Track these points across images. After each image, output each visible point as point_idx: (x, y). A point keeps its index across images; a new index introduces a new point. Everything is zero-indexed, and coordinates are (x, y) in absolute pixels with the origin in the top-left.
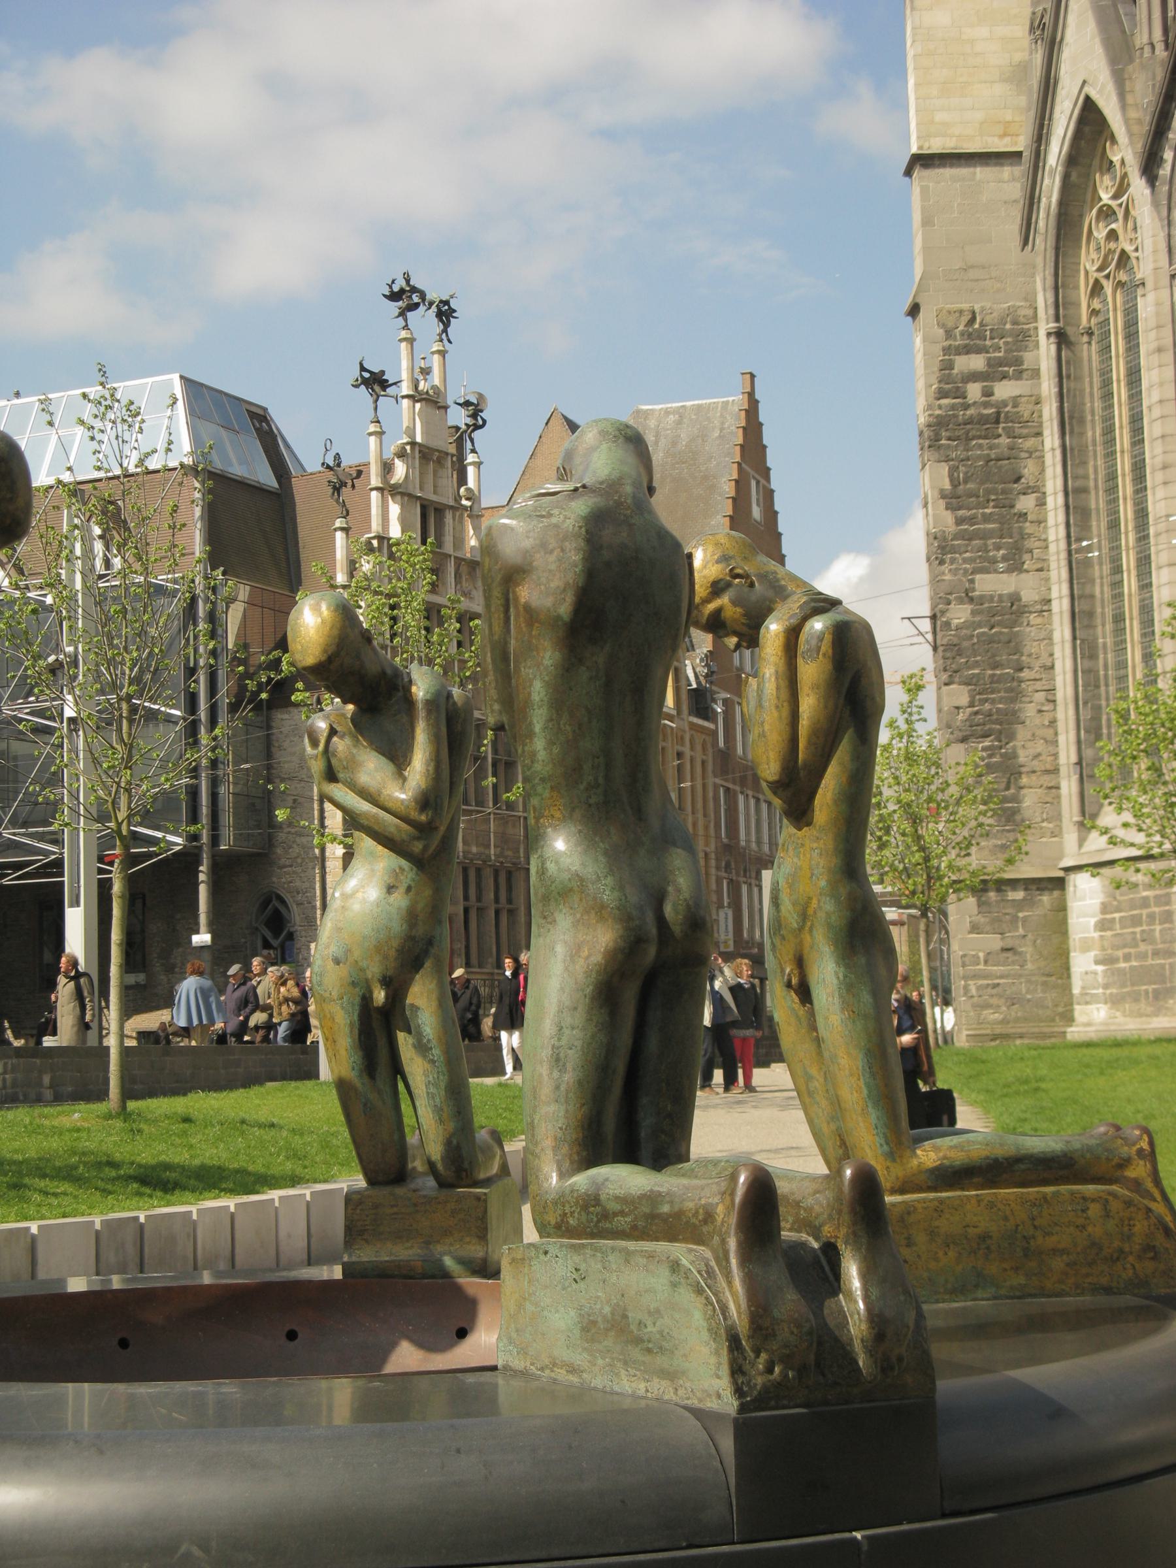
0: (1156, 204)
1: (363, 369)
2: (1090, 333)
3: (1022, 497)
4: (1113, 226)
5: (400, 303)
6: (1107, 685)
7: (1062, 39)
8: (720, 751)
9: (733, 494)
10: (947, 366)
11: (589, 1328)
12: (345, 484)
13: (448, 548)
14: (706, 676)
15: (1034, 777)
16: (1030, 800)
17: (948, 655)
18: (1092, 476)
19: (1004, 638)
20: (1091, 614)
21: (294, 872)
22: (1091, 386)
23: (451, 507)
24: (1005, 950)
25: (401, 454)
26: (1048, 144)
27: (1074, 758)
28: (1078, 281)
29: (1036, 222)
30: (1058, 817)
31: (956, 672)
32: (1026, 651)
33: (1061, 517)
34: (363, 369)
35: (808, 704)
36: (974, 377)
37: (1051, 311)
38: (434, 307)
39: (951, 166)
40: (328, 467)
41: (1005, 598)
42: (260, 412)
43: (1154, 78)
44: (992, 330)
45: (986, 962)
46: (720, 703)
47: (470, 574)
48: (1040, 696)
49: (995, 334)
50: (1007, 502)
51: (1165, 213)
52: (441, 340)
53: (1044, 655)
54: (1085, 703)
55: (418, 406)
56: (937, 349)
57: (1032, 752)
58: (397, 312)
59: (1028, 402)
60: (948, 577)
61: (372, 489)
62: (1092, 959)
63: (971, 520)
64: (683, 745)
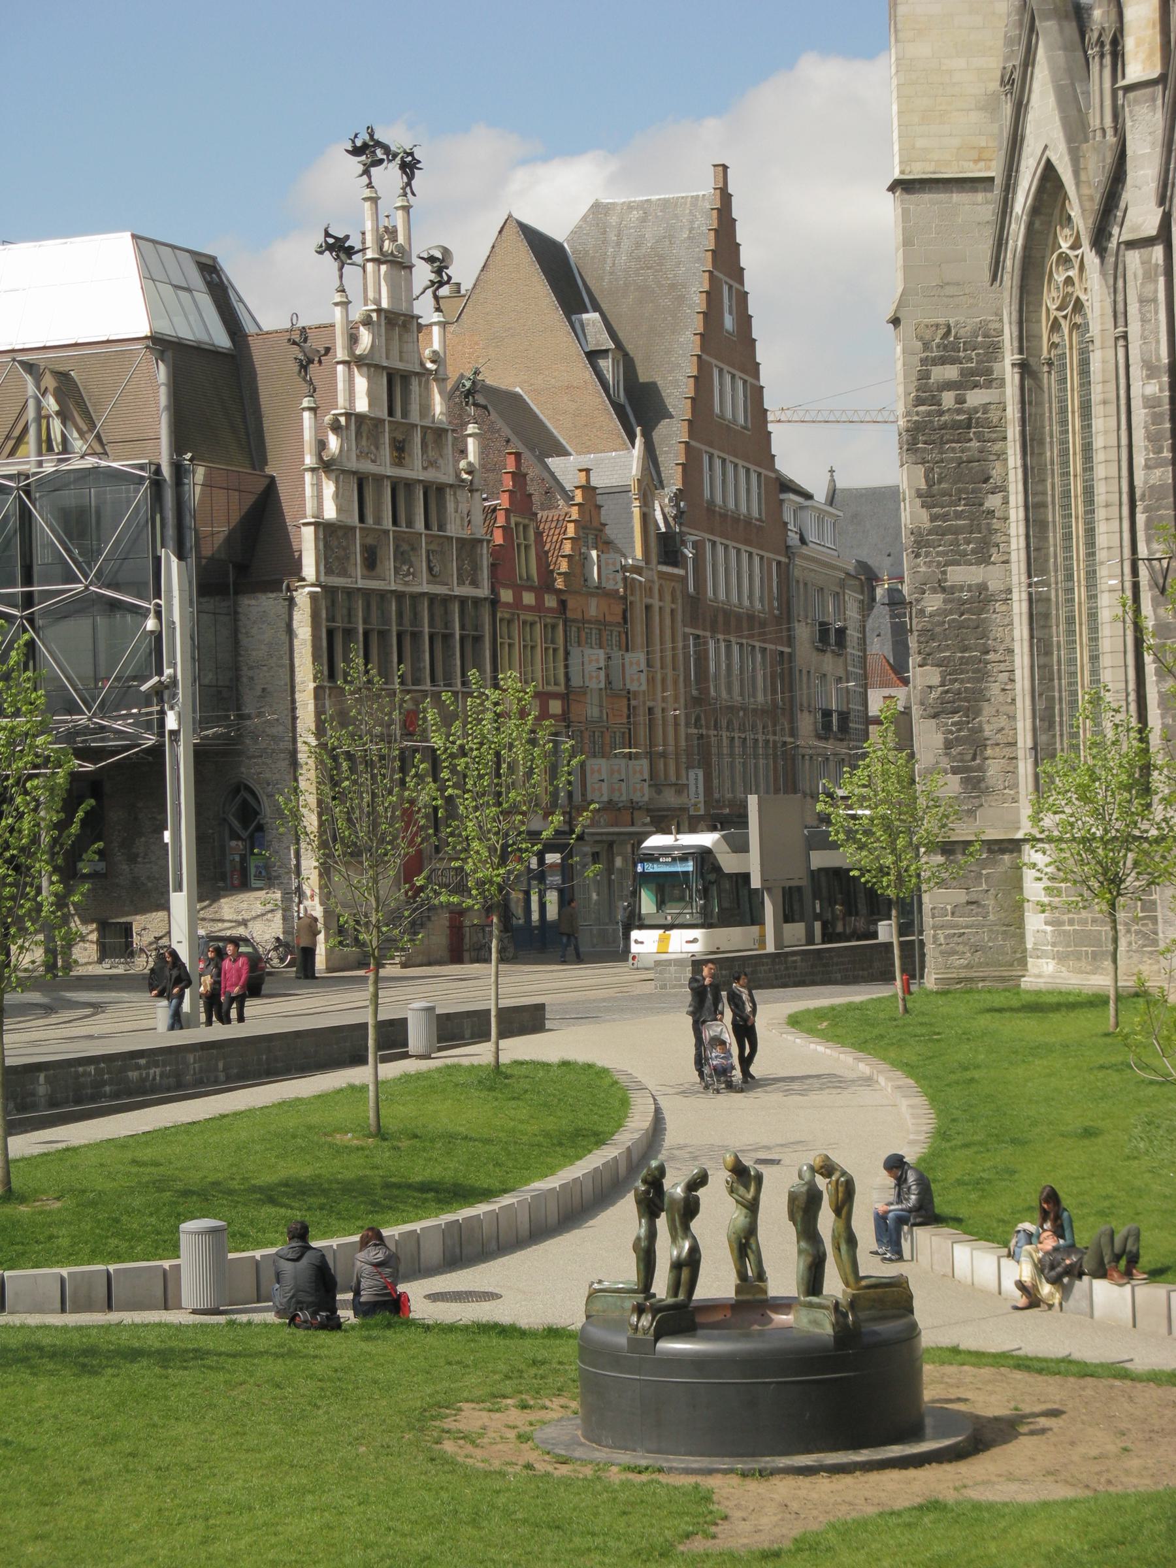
0: (1103, 273)
1: (327, 235)
2: (1050, 364)
3: (990, 496)
4: (1070, 273)
5: (363, 158)
6: (1060, 679)
7: (1028, 101)
8: (689, 596)
9: (703, 308)
10: (924, 376)
11: (810, 1322)
12: (311, 361)
13: (415, 417)
14: (675, 518)
15: (997, 749)
16: (994, 770)
17: (922, 639)
18: (1050, 493)
19: (971, 624)
20: (1047, 616)
21: (264, 763)
22: (1050, 410)
23: (417, 374)
24: (969, 903)
25: (367, 322)
26: (1014, 193)
27: (1030, 744)
28: (1040, 316)
29: (1004, 261)
30: (1015, 786)
31: (929, 655)
32: (992, 636)
33: (1022, 530)
34: (327, 235)
35: (840, 1195)
36: (948, 386)
37: (1016, 344)
38: (398, 158)
39: (930, 191)
40: (295, 343)
41: (974, 588)
42: (210, 262)
43: (1104, 161)
44: (965, 343)
45: (953, 914)
46: (690, 545)
47: (435, 442)
48: (1004, 677)
49: (968, 346)
50: (977, 500)
51: (1111, 282)
52: (405, 195)
53: (1008, 639)
54: (1041, 695)
55: (383, 268)
56: (916, 360)
57: (996, 726)
58: (361, 168)
59: (997, 409)
60: (923, 569)
61: (338, 363)
62: (1043, 920)
63: (944, 517)
64: (651, 597)
